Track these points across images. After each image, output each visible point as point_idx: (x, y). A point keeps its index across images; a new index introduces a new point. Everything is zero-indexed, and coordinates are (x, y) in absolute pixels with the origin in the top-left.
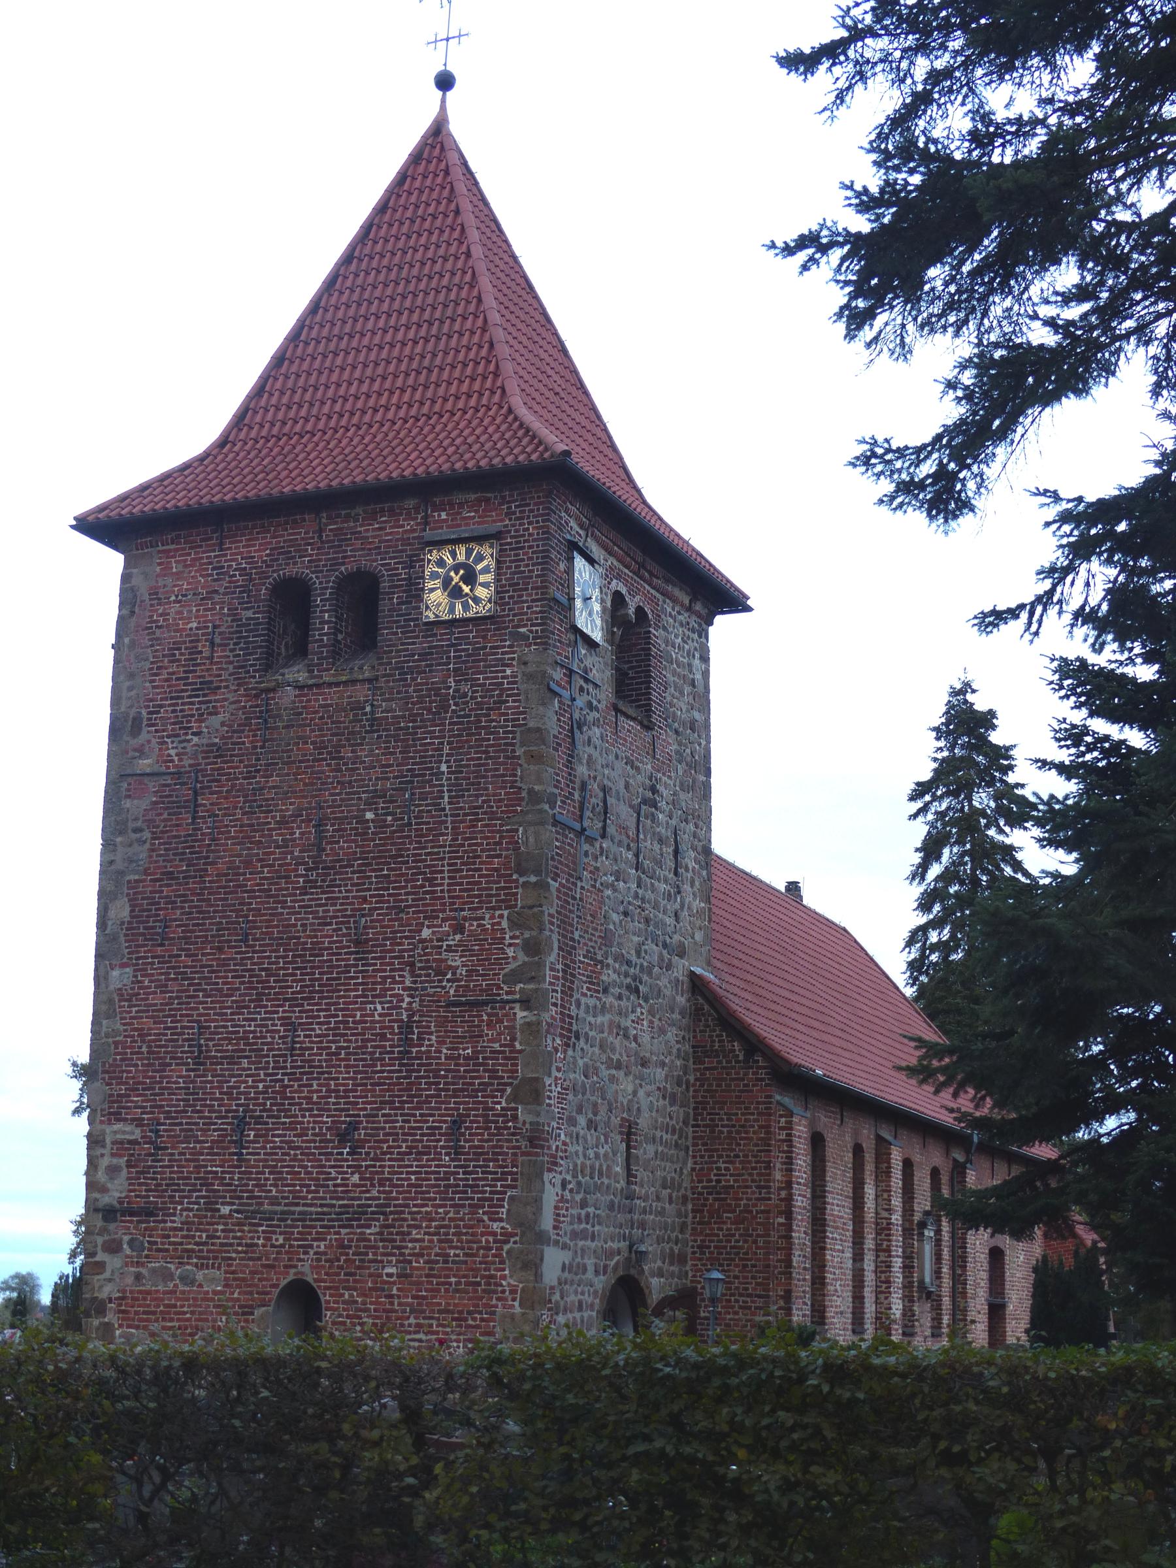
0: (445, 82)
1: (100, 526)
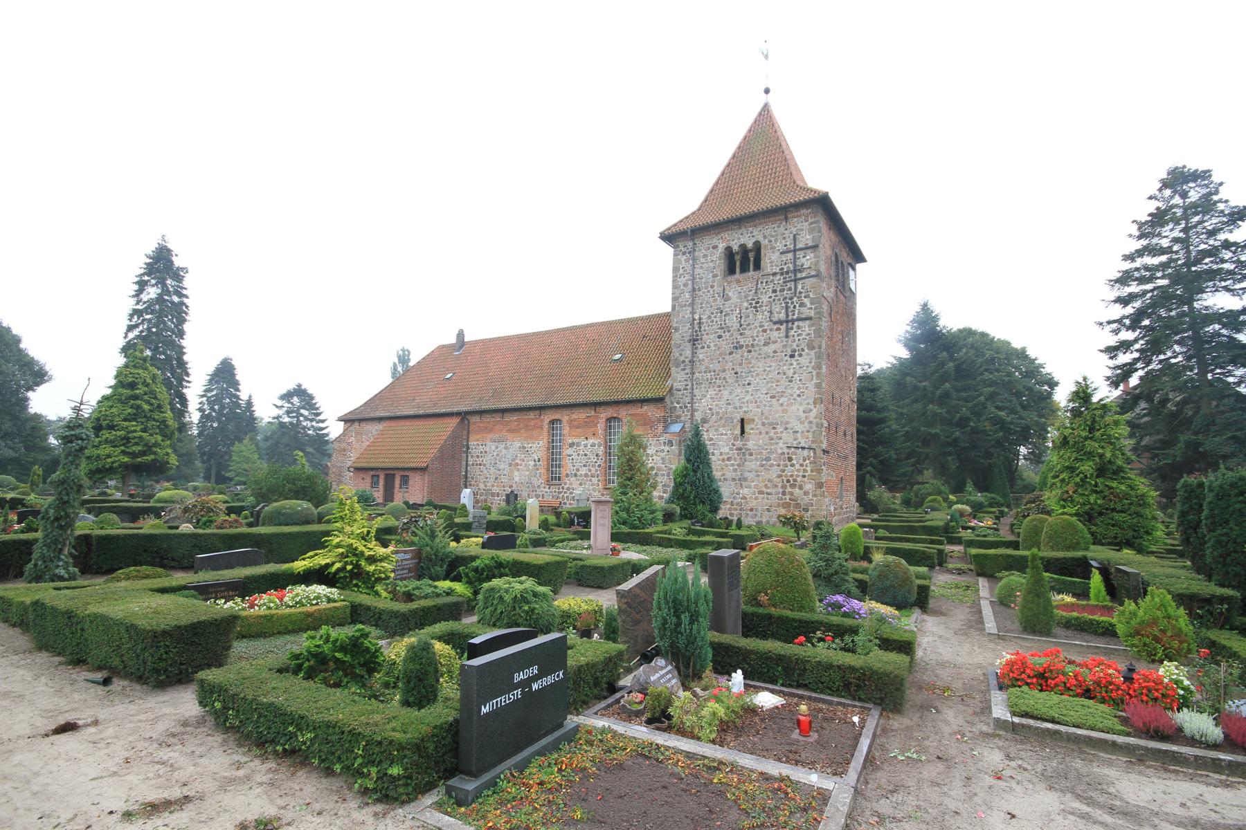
0: (767, 91)
1: (669, 237)
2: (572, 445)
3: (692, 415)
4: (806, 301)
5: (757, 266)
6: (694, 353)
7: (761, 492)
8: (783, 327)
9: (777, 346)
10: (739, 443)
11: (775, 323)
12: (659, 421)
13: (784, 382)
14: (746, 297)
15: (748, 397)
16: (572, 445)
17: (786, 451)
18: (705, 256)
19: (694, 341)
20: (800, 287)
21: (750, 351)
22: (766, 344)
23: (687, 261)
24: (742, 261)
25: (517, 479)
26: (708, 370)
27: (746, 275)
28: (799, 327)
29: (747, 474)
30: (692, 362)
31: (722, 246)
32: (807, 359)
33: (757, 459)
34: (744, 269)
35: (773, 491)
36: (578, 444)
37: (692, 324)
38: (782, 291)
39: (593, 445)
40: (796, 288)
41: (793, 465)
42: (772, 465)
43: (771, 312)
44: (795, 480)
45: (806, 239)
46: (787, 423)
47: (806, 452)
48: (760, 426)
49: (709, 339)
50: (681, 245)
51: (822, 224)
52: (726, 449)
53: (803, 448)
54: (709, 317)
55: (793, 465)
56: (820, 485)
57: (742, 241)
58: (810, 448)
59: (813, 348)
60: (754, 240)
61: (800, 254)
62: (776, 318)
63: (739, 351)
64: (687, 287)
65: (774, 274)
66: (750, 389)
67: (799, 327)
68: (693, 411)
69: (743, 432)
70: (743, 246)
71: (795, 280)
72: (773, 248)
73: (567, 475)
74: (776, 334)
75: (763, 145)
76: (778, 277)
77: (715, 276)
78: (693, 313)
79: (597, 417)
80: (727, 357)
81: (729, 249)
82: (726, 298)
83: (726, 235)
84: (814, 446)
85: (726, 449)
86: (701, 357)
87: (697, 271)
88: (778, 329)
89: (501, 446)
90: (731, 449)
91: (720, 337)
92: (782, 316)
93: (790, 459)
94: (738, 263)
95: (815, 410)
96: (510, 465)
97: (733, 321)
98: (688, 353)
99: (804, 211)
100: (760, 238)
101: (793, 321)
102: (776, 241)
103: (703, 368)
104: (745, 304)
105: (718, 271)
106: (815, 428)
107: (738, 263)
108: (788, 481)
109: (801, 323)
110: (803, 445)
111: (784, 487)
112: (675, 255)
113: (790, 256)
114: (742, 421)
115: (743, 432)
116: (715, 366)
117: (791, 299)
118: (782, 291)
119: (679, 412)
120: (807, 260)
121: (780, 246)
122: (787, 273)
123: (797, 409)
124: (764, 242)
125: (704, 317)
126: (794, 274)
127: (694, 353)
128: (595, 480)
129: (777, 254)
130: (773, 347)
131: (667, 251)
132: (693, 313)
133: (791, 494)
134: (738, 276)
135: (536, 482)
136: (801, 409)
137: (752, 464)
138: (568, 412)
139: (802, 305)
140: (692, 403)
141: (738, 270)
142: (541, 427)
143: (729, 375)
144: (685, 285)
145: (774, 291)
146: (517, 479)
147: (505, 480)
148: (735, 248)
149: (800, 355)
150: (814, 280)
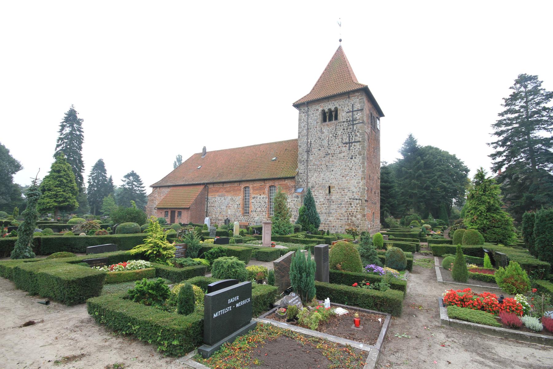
1: (297, 105)
2: (254, 198)
3: (307, 185)
4: (358, 134)
5: (336, 118)
6: (308, 157)
7: (338, 219)
8: (348, 145)
9: (345, 154)
10: (328, 197)
11: (344, 144)
12: (292, 187)
13: (348, 170)
14: (331, 132)
15: (332, 177)
16: (254, 198)
17: (349, 200)
18: (313, 114)
19: (308, 152)
20: (355, 127)
21: (333, 156)
22: (340, 153)
23: (305, 116)
24: (329, 116)
25: (229, 213)
26: (314, 165)
27: (331, 122)
28: (354, 145)
29: (331, 211)
30: (307, 161)
31: (320, 109)
32: (358, 159)
33: (336, 204)
34: (330, 120)
35: (343, 218)
36: (257, 198)
37: (307, 144)
38: (347, 129)
39: (263, 198)
40: (353, 128)
41: (352, 207)
42: (343, 207)
43: (342, 139)
44: (353, 214)
45: (358, 106)
46: (350, 188)
47: (358, 201)
48: (337, 189)
49: (315, 151)
50: (302, 109)
51: (365, 99)
52: (322, 200)
53: (356, 199)
54: (315, 141)
55: (352, 207)
56: (364, 216)
57: (329, 107)
58: (359, 199)
59: (361, 155)
60: (334, 107)
61: (355, 113)
62: (344, 141)
63: (328, 156)
64: (305, 128)
65: (344, 122)
66: (333, 173)
67: (354, 145)
68: (308, 183)
69: (330, 192)
70: (330, 110)
71: (353, 125)
72: (343, 110)
73: (252, 211)
74: (344, 148)
75: (339, 65)
76: (345, 123)
77: (317, 123)
78: (308, 139)
79: (265, 186)
80: (323, 159)
81: (323, 111)
82: (322, 132)
83: (322, 104)
84: (361, 198)
85: (322, 200)
86: (311, 159)
87: (309, 120)
88: (345, 146)
89: (223, 198)
90: (324, 200)
91: (319, 150)
92: (347, 141)
93: (351, 204)
94: (327, 117)
95: (362, 182)
96: (226, 207)
97: (325, 143)
98: (305, 157)
99: (357, 94)
100: (337, 106)
101: (352, 143)
102: (344, 107)
103: (312, 164)
104: (331, 135)
105: (319, 121)
106: (362, 190)
107: (327, 117)
108: (350, 214)
109: (355, 144)
110: (356, 198)
111: (348, 216)
112: (300, 113)
113: (351, 114)
114: (329, 187)
115: (330, 192)
116: (317, 163)
117: (351, 133)
118: (347, 129)
119: (301, 183)
120: (358, 116)
121: (346, 109)
122: (349, 121)
123: (354, 182)
124: (339, 108)
125: (313, 141)
126: (352, 122)
127: (308, 157)
128: (264, 213)
129: (345, 113)
130: (343, 154)
131: (296, 111)
132: (308, 139)
133: (351, 219)
134: (327, 122)
135: (238, 214)
136: (356, 182)
137: (334, 206)
138: (252, 183)
139: (356, 136)
140: (307, 179)
141: (327, 120)
142: (240, 190)
143: (323, 167)
144: (304, 127)
145: (344, 129)
146: (229, 213)
147: (224, 213)
148: (326, 110)
149: (355, 158)
150: (361, 124)
